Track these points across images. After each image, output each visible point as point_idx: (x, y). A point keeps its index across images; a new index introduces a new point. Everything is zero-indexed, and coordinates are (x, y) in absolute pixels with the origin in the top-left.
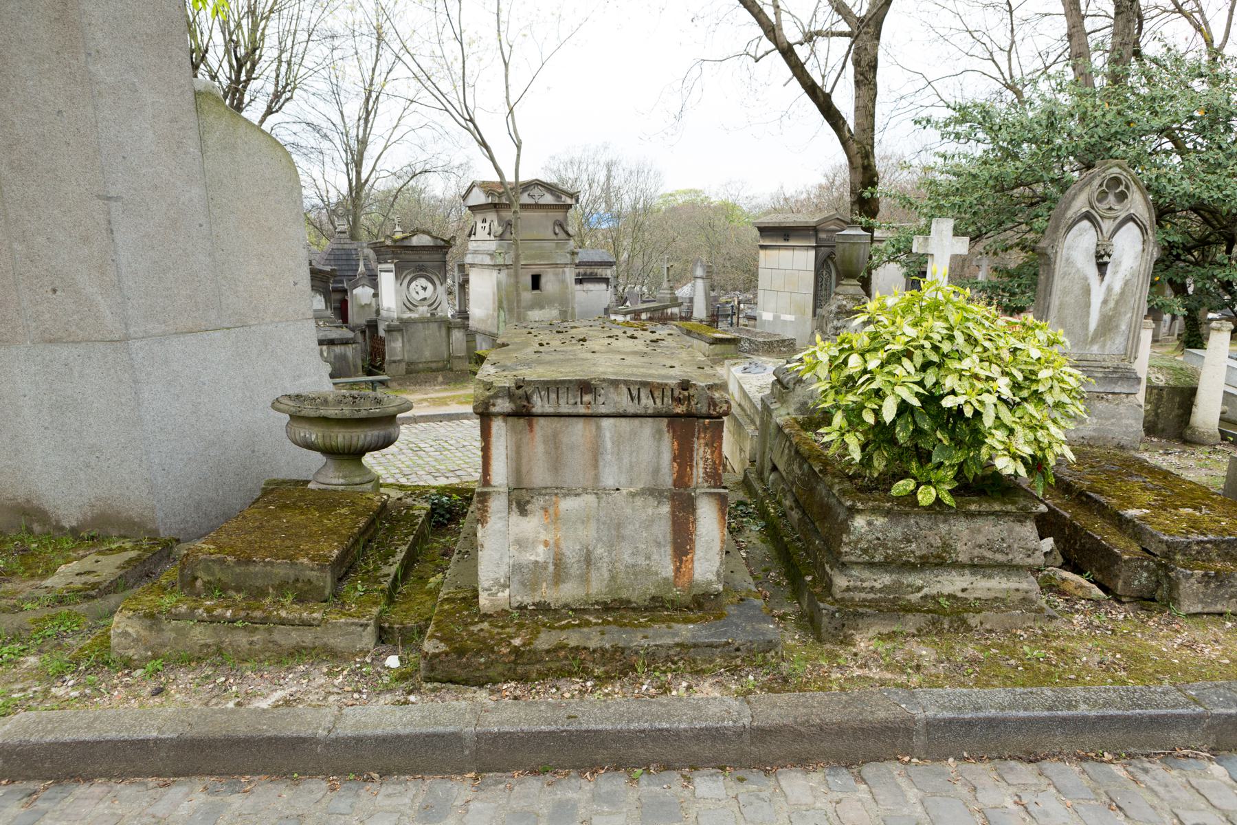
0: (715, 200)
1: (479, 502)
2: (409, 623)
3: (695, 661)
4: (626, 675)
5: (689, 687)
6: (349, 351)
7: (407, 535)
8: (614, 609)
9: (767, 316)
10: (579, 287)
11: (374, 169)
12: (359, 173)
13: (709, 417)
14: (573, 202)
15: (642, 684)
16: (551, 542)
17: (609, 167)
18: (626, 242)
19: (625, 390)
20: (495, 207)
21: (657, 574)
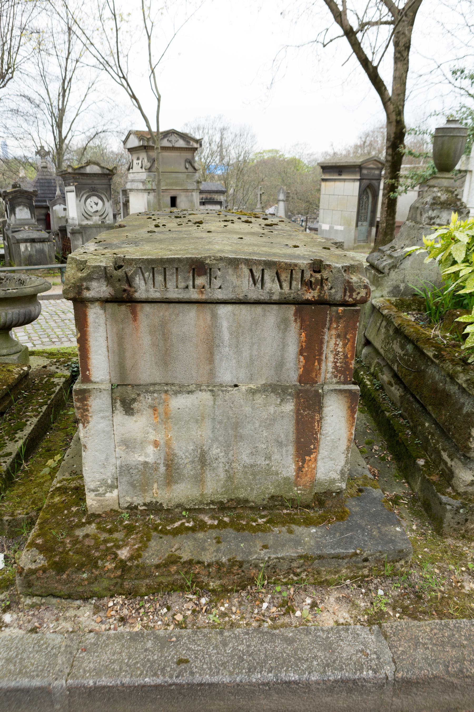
0: (288, 156)
1: (78, 400)
2: (20, 514)
3: (319, 573)
4: (244, 588)
5: (314, 605)
6: (46, 246)
7: (41, 405)
8: (233, 511)
9: (325, 227)
10: (202, 207)
11: (70, 129)
12: (60, 132)
13: (344, 304)
14: (198, 146)
15: (262, 601)
16: (162, 442)
17: (223, 130)
18: (232, 182)
19: (246, 272)
20: (145, 148)
21: (277, 474)
